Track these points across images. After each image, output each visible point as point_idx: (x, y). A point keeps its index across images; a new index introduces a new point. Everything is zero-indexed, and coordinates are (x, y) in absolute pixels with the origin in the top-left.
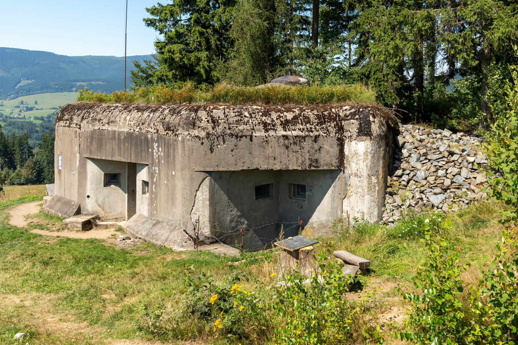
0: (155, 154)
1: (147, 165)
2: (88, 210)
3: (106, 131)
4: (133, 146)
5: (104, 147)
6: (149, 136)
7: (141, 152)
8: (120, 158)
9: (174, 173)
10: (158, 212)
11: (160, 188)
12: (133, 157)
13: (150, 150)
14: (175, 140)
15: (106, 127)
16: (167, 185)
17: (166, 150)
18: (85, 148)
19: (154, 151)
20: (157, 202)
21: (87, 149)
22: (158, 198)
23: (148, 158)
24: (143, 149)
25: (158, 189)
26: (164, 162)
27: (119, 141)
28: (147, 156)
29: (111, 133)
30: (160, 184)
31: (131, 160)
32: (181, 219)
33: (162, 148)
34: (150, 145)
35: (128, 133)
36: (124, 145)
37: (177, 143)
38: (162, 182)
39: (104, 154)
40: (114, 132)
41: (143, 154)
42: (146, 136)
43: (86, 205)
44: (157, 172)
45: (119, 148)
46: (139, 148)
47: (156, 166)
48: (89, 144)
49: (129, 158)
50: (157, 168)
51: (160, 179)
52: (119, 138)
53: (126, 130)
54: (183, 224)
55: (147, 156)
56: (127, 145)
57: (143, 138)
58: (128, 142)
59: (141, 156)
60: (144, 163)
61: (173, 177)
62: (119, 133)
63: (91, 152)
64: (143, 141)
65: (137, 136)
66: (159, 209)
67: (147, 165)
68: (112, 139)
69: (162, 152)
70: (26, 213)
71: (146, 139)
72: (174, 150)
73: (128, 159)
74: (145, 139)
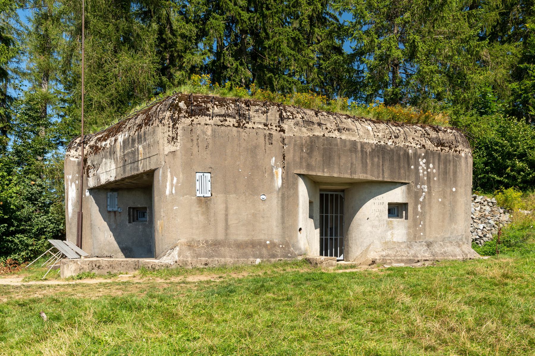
0: (421, 171)
1: (405, 184)
2: (300, 249)
3: (339, 140)
4: (387, 164)
5: (336, 160)
6: (410, 151)
7: (399, 168)
8: (365, 175)
9: (454, 189)
10: (427, 233)
11: (430, 207)
12: (386, 175)
13: (412, 167)
14: (457, 156)
15: (336, 134)
16: (442, 203)
17: (442, 166)
18: (298, 160)
19: (420, 168)
20: (424, 222)
21: (301, 162)
22: (428, 217)
23: (409, 176)
24: (402, 165)
25: (427, 208)
26: (439, 179)
27: (362, 155)
28: (407, 173)
29: (348, 143)
30: (430, 203)
31: (383, 178)
32: (464, 233)
33: (434, 164)
34: (412, 161)
35: (376, 145)
36: (372, 160)
37: (460, 159)
38: (434, 201)
39: (336, 170)
40: (354, 143)
41: (402, 171)
42: (405, 151)
43: (297, 241)
44: (426, 190)
45: (362, 163)
46: (396, 164)
47: (423, 184)
48: (305, 155)
49: (381, 175)
50: (426, 186)
51: (430, 198)
52: (362, 151)
53: (375, 142)
54: (466, 239)
55: (407, 173)
56: (376, 160)
57: (402, 153)
58: (378, 156)
59: (399, 174)
60: (403, 181)
61: (453, 194)
62: (363, 145)
63: (309, 166)
64: (402, 157)
65: (392, 150)
66: (428, 229)
67: (405, 184)
68: (350, 151)
69: (434, 168)
70: (132, 205)
71: (406, 154)
72: (455, 166)
73: (378, 177)
74: (404, 154)
